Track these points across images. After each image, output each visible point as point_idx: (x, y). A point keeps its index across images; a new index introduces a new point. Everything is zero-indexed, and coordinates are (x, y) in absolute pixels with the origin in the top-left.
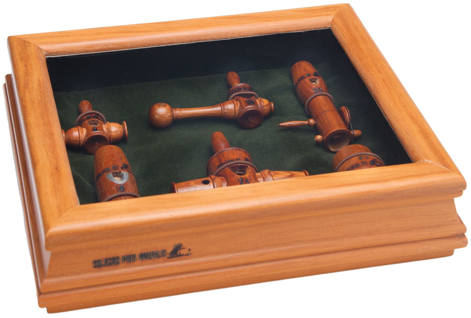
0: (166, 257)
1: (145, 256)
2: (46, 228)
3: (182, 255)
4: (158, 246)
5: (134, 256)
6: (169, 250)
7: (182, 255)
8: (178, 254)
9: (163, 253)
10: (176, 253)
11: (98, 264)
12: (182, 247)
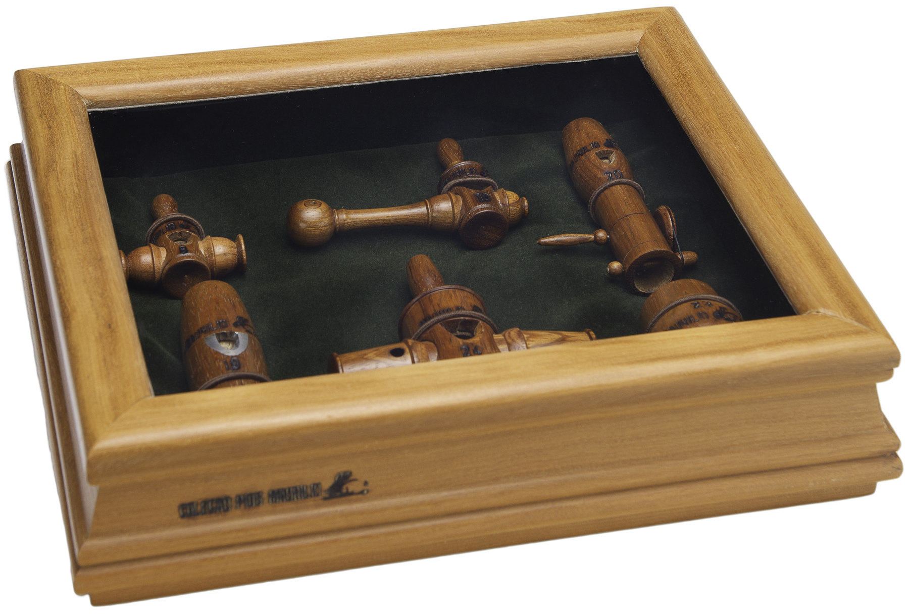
0: (320, 497)
1: (280, 496)
2: (90, 441)
3: (352, 494)
4: (306, 476)
5: (258, 495)
6: (327, 484)
7: (352, 494)
8: (344, 490)
9: (315, 490)
10: (339, 489)
11: (189, 511)
12: (352, 478)
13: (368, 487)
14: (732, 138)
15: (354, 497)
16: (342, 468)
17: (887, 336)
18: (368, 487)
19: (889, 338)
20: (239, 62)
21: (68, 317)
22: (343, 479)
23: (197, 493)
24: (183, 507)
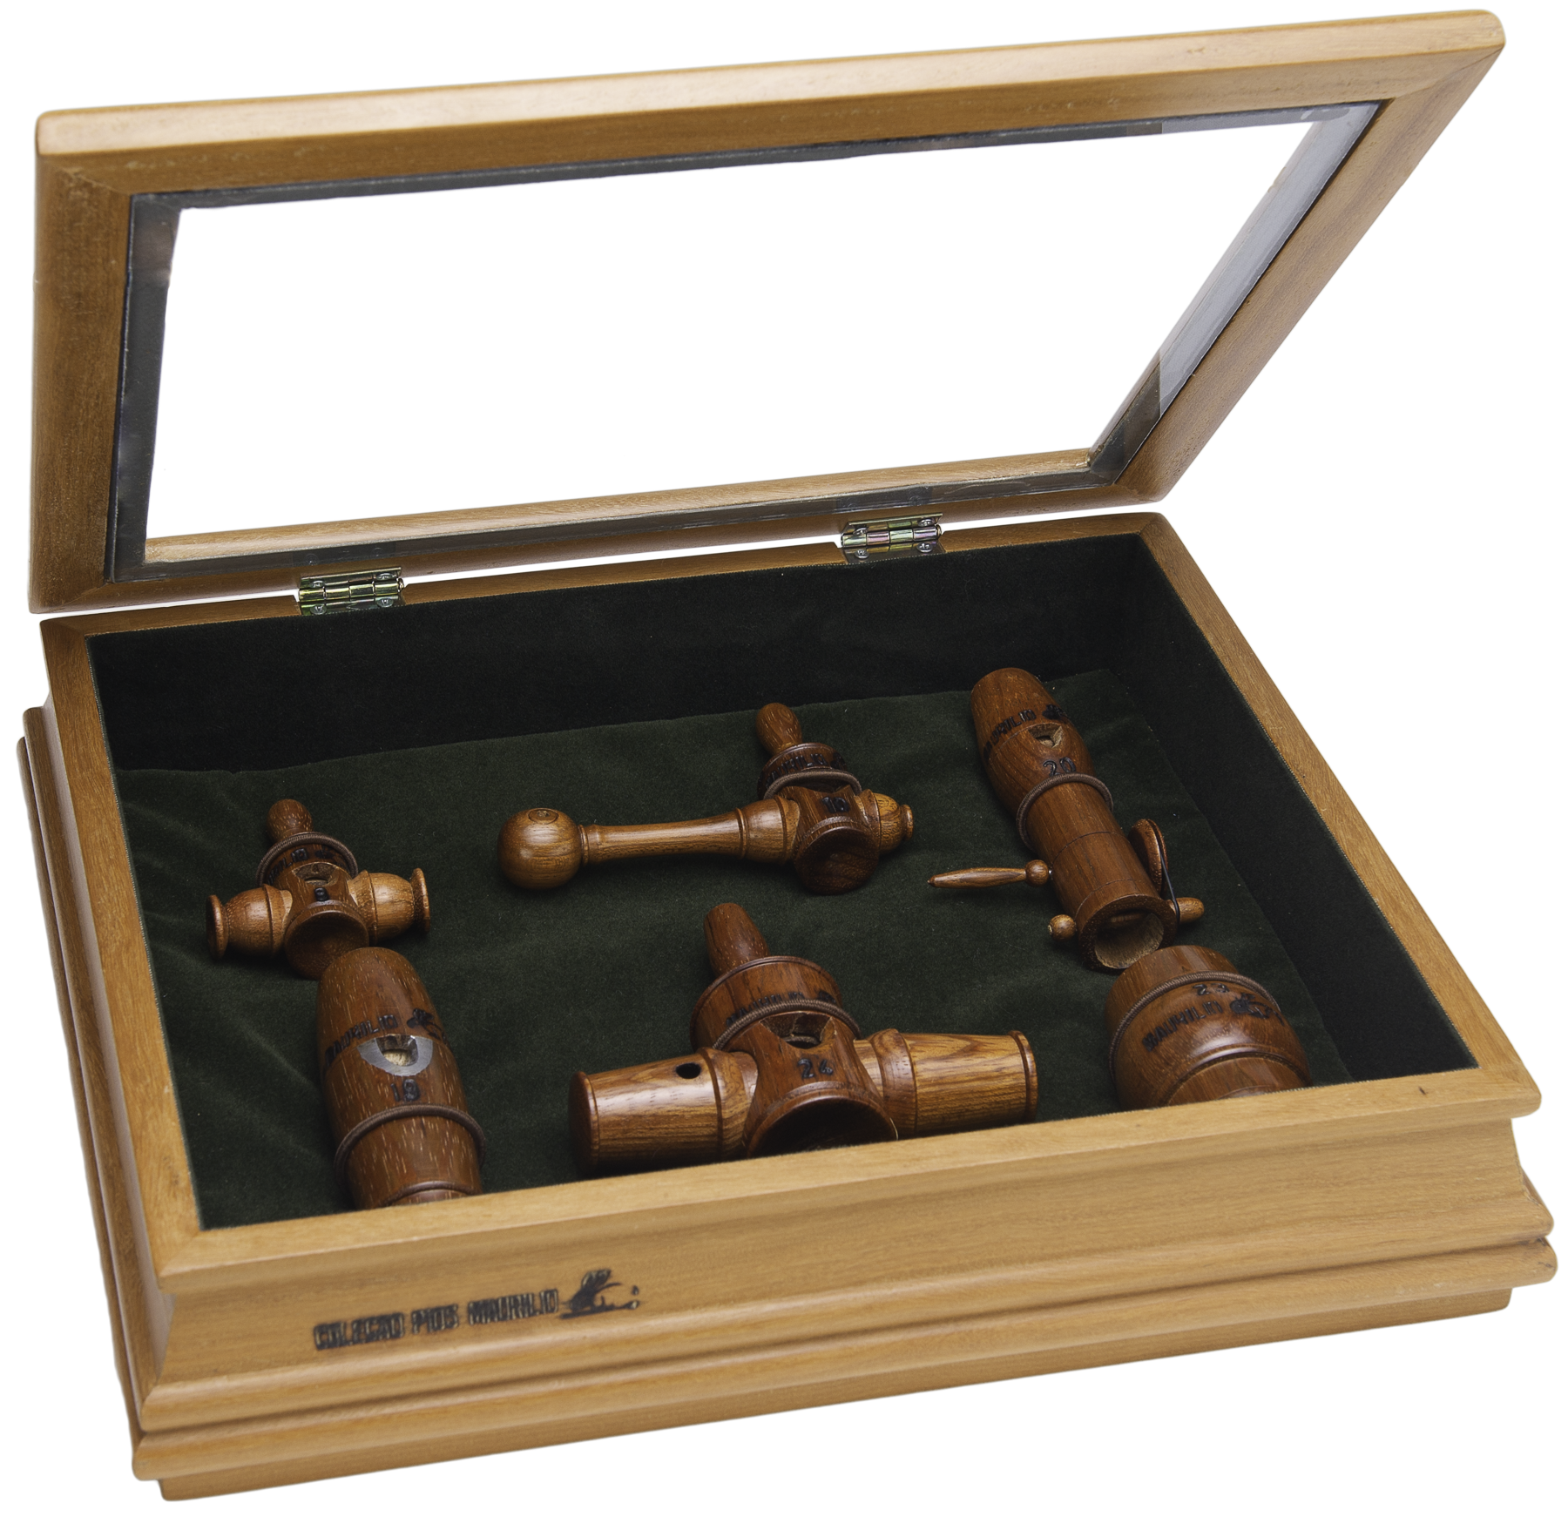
1: (487, 1312)
3: (612, 1308)
4: (531, 1282)
6: (568, 1292)
7: (612, 1308)
8: (598, 1303)
10: (589, 1300)
11: (331, 1338)
16: (595, 1264)
22: (596, 1283)
23: (349, 1307)
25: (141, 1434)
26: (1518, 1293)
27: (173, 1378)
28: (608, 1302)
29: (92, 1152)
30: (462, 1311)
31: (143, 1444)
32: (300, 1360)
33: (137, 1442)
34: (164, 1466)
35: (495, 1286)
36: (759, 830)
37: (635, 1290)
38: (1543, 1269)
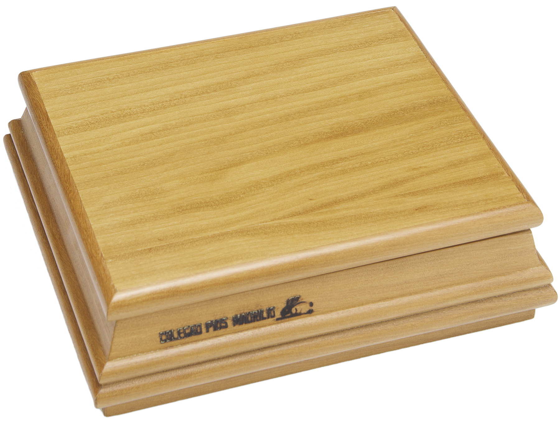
1: (241, 320)
2: (108, 292)
3: (300, 314)
4: (265, 301)
6: (281, 306)
7: (300, 314)
8: (294, 311)
9: (270, 312)
10: (289, 311)
11: (168, 337)
12: (300, 300)
13: (313, 308)
14: (229, 109)
15: (302, 316)
16: (291, 294)
17: (547, 269)
18: (313, 308)
19: (545, 266)
20: (420, 209)
21: (44, 237)
22: (293, 302)
23: (174, 324)
24: (165, 333)
25: (98, 386)
26: (538, 311)
27: (117, 357)
28: (298, 311)
29: (70, 311)
30: (230, 323)
31: (102, 391)
32: (155, 350)
33: (96, 392)
34: (105, 403)
35: (248, 305)
36: (114, 303)
37: (311, 304)
38: (551, 298)
